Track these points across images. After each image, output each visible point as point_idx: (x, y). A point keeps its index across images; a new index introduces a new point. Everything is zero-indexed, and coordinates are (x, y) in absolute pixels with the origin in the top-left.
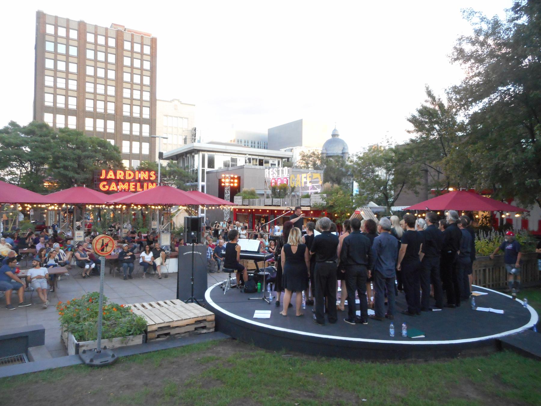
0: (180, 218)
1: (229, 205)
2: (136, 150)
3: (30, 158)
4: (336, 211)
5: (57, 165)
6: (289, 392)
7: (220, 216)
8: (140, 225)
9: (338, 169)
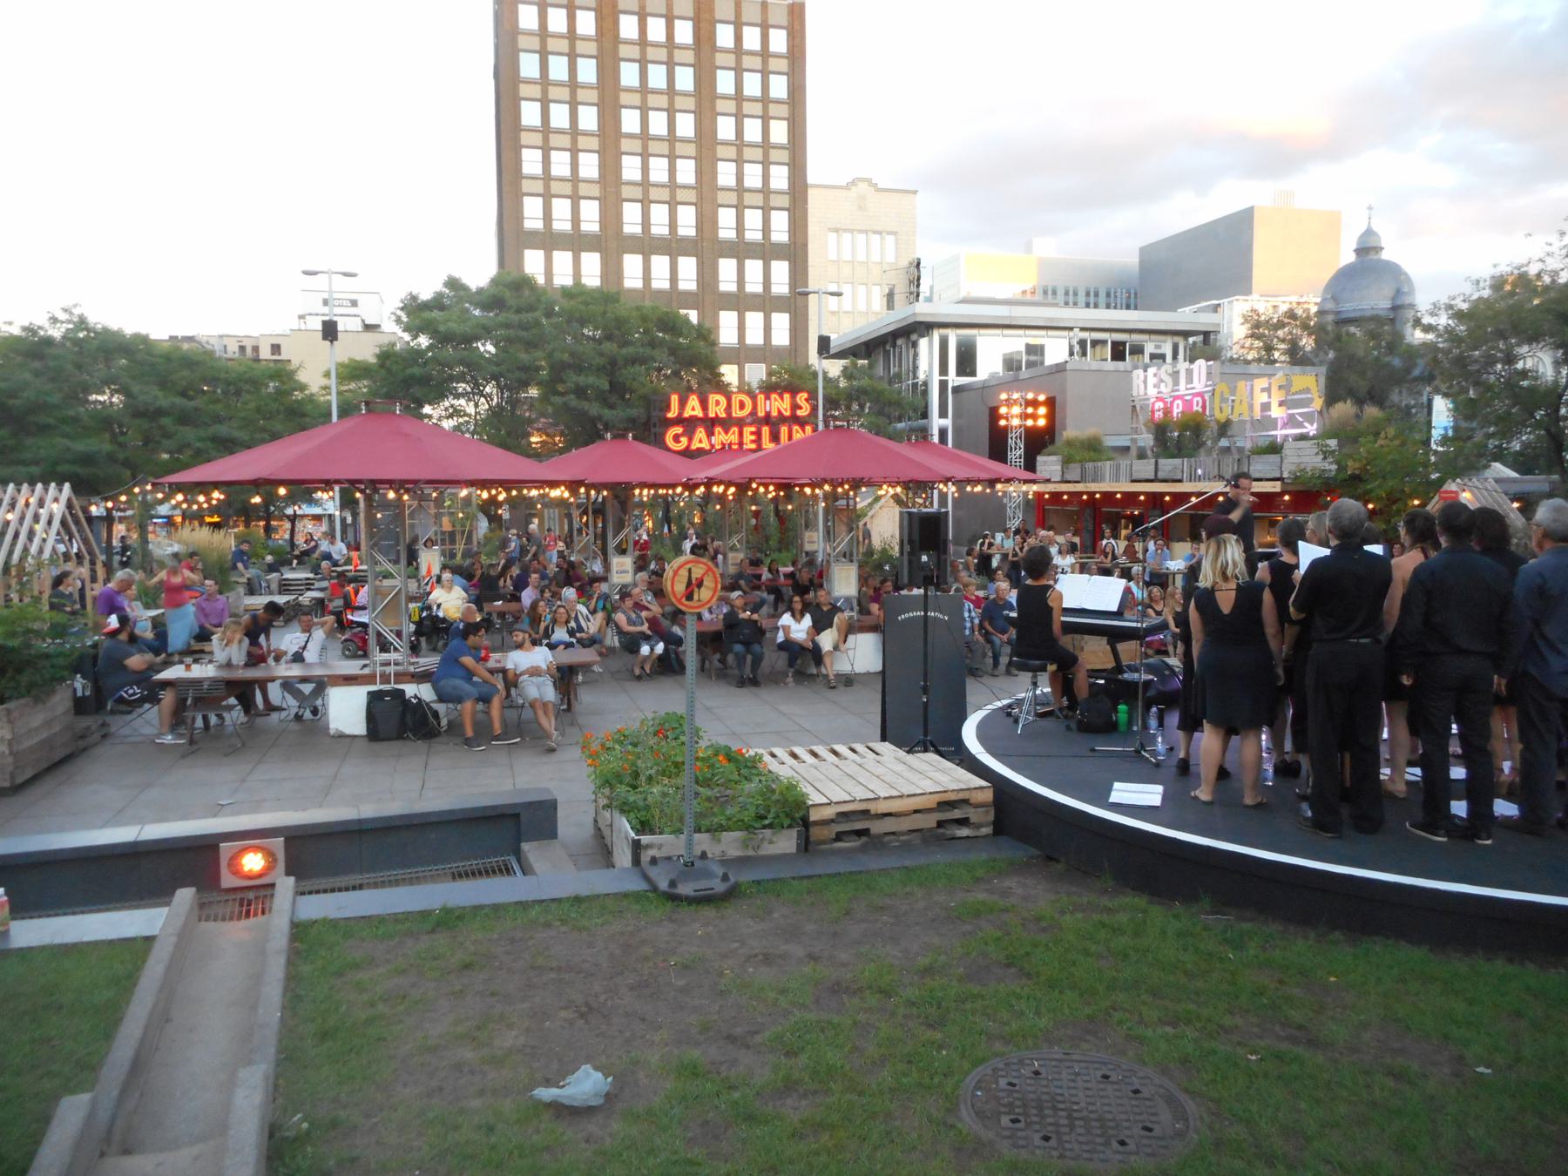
0: (885, 524)
1: (1026, 482)
2: (755, 337)
3: (496, 371)
4: (1371, 490)
5: (561, 388)
6: (1228, 1021)
7: (993, 514)
8: (773, 543)
9: (1377, 359)
